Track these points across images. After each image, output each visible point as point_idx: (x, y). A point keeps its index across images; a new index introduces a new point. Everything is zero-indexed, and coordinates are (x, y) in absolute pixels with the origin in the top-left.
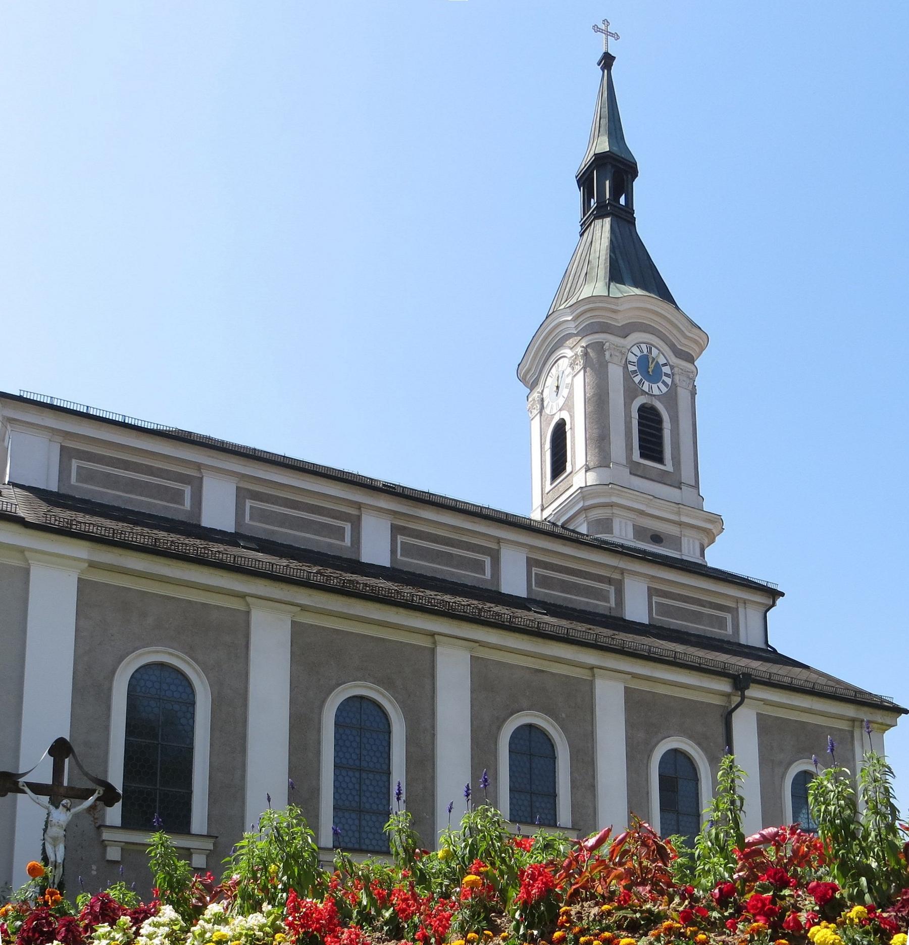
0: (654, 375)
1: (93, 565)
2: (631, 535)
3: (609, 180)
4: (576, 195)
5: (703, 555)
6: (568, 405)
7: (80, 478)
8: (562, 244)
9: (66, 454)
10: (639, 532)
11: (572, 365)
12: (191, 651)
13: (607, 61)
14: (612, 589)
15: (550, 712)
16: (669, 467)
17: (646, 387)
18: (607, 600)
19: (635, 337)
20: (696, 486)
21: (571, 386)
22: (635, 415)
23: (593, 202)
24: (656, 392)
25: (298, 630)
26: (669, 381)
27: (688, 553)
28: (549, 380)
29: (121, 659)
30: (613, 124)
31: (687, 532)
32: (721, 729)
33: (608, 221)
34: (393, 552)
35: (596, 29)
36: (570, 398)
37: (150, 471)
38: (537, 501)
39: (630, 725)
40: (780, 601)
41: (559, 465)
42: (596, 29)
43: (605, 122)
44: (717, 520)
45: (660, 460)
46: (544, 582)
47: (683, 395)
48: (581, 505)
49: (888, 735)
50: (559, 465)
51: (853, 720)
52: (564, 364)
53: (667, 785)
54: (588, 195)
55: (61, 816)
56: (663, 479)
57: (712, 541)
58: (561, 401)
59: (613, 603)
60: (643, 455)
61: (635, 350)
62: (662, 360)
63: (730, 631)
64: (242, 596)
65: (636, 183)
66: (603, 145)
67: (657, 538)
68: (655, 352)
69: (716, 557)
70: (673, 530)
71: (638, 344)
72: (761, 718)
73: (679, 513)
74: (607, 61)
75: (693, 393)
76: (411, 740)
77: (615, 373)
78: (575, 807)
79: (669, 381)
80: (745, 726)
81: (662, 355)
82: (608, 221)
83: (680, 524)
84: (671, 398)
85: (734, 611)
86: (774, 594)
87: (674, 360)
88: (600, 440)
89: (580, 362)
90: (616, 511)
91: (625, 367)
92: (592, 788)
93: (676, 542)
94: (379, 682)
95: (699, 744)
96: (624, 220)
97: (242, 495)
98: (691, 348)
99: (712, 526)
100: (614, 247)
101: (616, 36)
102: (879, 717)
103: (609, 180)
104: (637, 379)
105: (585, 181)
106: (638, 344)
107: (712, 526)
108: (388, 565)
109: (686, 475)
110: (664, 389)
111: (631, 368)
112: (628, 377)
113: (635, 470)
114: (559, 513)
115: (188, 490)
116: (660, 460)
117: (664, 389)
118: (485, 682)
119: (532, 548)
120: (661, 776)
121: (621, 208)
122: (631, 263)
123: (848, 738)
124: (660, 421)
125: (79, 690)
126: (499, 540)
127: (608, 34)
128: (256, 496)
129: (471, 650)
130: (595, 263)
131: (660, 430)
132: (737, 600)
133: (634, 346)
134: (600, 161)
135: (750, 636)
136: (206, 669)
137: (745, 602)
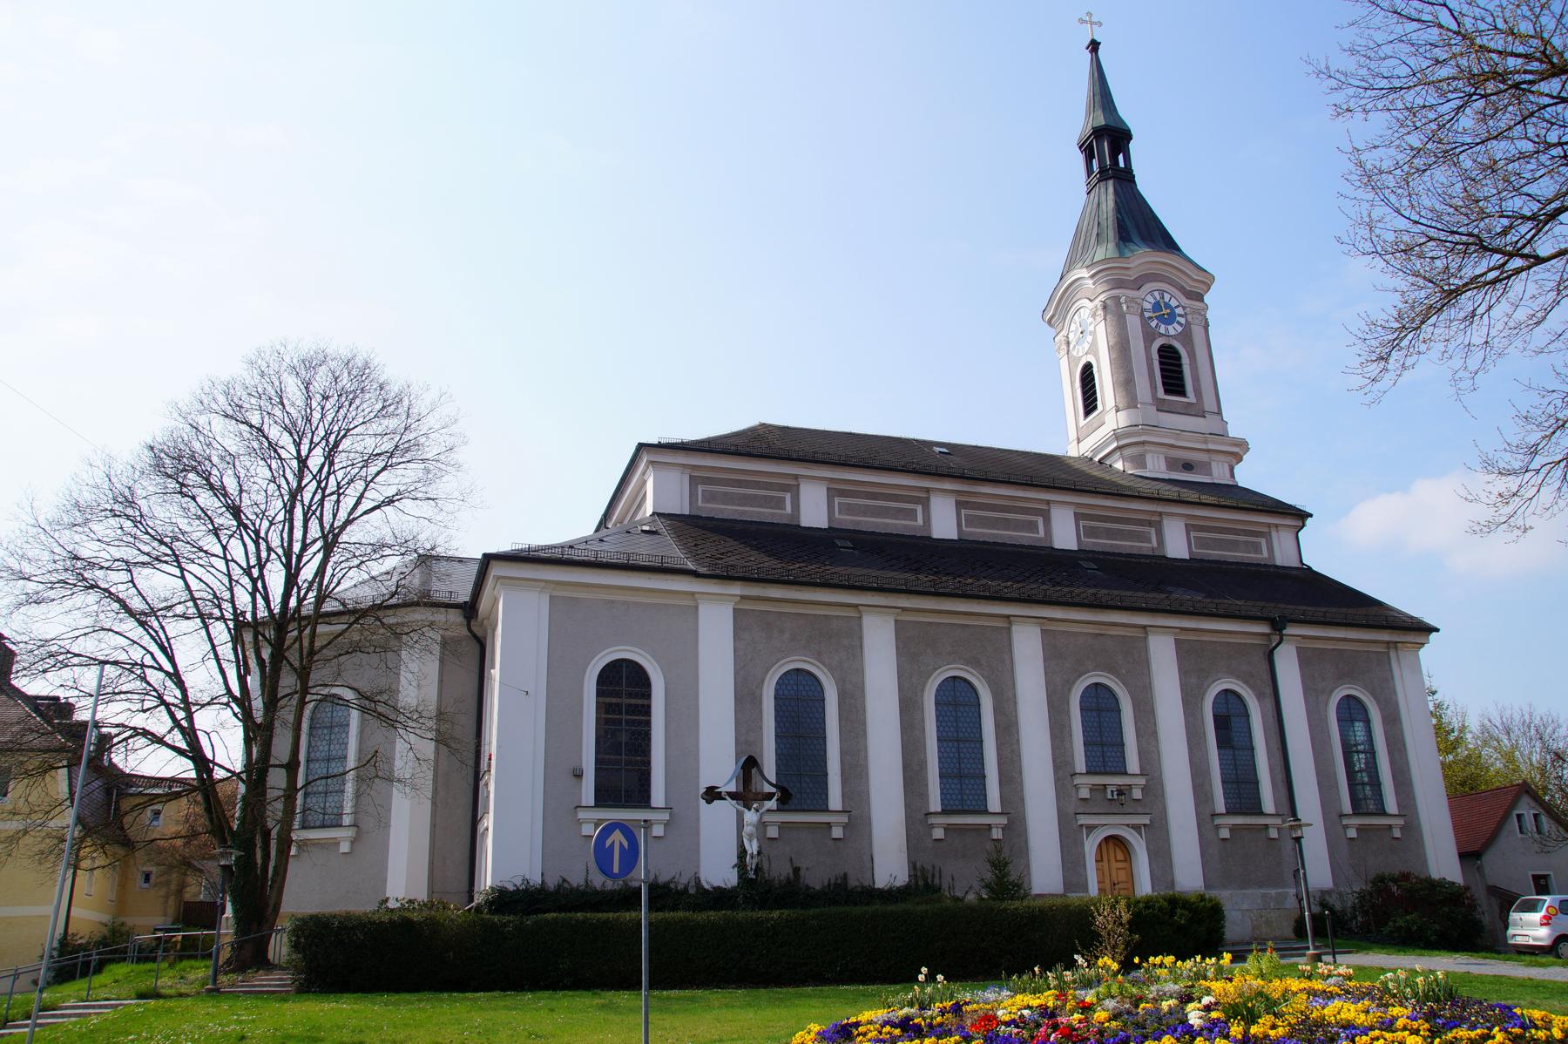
0: (1170, 319)
1: (743, 597)
2: (1163, 466)
3: (1108, 144)
4: (1079, 158)
5: (1232, 475)
6: (1093, 349)
7: (705, 500)
8: (1068, 189)
9: (694, 481)
10: (1172, 464)
11: (1094, 315)
12: (819, 656)
13: (1094, 46)
14: (1153, 531)
15: (1111, 669)
16: (1191, 397)
17: (1162, 330)
18: (1149, 541)
19: (1148, 287)
20: (1219, 413)
21: (1094, 333)
22: (1155, 356)
23: (1095, 162)
24: (1172, 332)
25: (900, 627)
26: (1182, 320)
27: (1219, 475)
28: (1073, 327)
29: (768, 670)
30: (1102, 94)
31: (1215, 457)
32: (1265, 666)
33: (1111, 183)
34: (959, 525)
35: (1082, 21)
36: (1094, 344)
37: (758, 485)
38: (1073, 435)
39: (1183, 672)
40: (1309, 521)
41: (1090, 404)
42: (1082, 21)
43: (1098, 98)
44: (1243, 445)
45: (1183, 393)
46: (1090, 532)
47: (1197, 331)
48: (1115, 445)
49: (1422, 652)
50: (1090, 404)
51: (1388, 643)
52: (1085, 313)
53: (1222, 723)
54: (1089, 158)
55: (750, 817)
56: (1188, 411)
57: (1240, 459)
58: (1086, 346)
59: (1155, 544)
60: (1167, 392)
61: (1150, 298)
62: (1173, 303)
63: (1265, 554)
64: (856, 606)
65: (1131, 145)
66: (1101, 121)
67: (1188, 467)
68: (1167, 297)
69: (1248, 476)
70: (1203, 457)
71: (1151, 293)
72: (1300, 651)
73: (1206, 442)
74: (1094, 46)
75: (1206, 326)
76: (997, 710)
77: (1134, 322)
78: (1142, 754)
79: (1182, 320)
80: (1287, 665)
81: (1174, 300)
82: (1111, 183)
83: (1208, 451)
84: (1186, 336)
85: (1267, 536)
86: (1301, 516)
87: (1185, 301)
88: (1126, 383)
89: (1100, 312)
90: (1147, 447)
91: (1142, 315)
92: (1154, 734)
93: (1206, 468)
94: (967, 663)
95: (1246, 682)
96: (1123, 178)
97: (832, 494)
98: (1198, 288)
99: (1237, 451)
100: (1118, 209)
101: (1100, 24)
102: (1411, 638)
103: (1108, 144)
104: (1153, 324)
105: (1088, 150)
106: (1151, 293)
107: (1237, 451)
108: (955, 537)
109: (1209, 404)
110: (1180, 329)
111: (1147, 315)
112: (1145, 322)
113: (1161, 407)
114: (1096, 451)
115: (788, 497)
116: (1183, 393)
117: (1180, 329)
118: (1053, 653)
119: (1078, 505)
120: (1215, 716)
121: (1121, 170)
122: (1136, 224)
123: (1384, 661)
124: (1179, 358)
125: (739, 699)
126: (1048, 502)
127: (1092, 23)
128: (842, 493)
129: (1042, 624)
130: (1104, 223)
131: (1180, 366)
132: (1269, 525)
133: (1148, 297)
134: (1098, 133)
135: (1283, 556)
136: (831, 669)
137: (1277, 526)
